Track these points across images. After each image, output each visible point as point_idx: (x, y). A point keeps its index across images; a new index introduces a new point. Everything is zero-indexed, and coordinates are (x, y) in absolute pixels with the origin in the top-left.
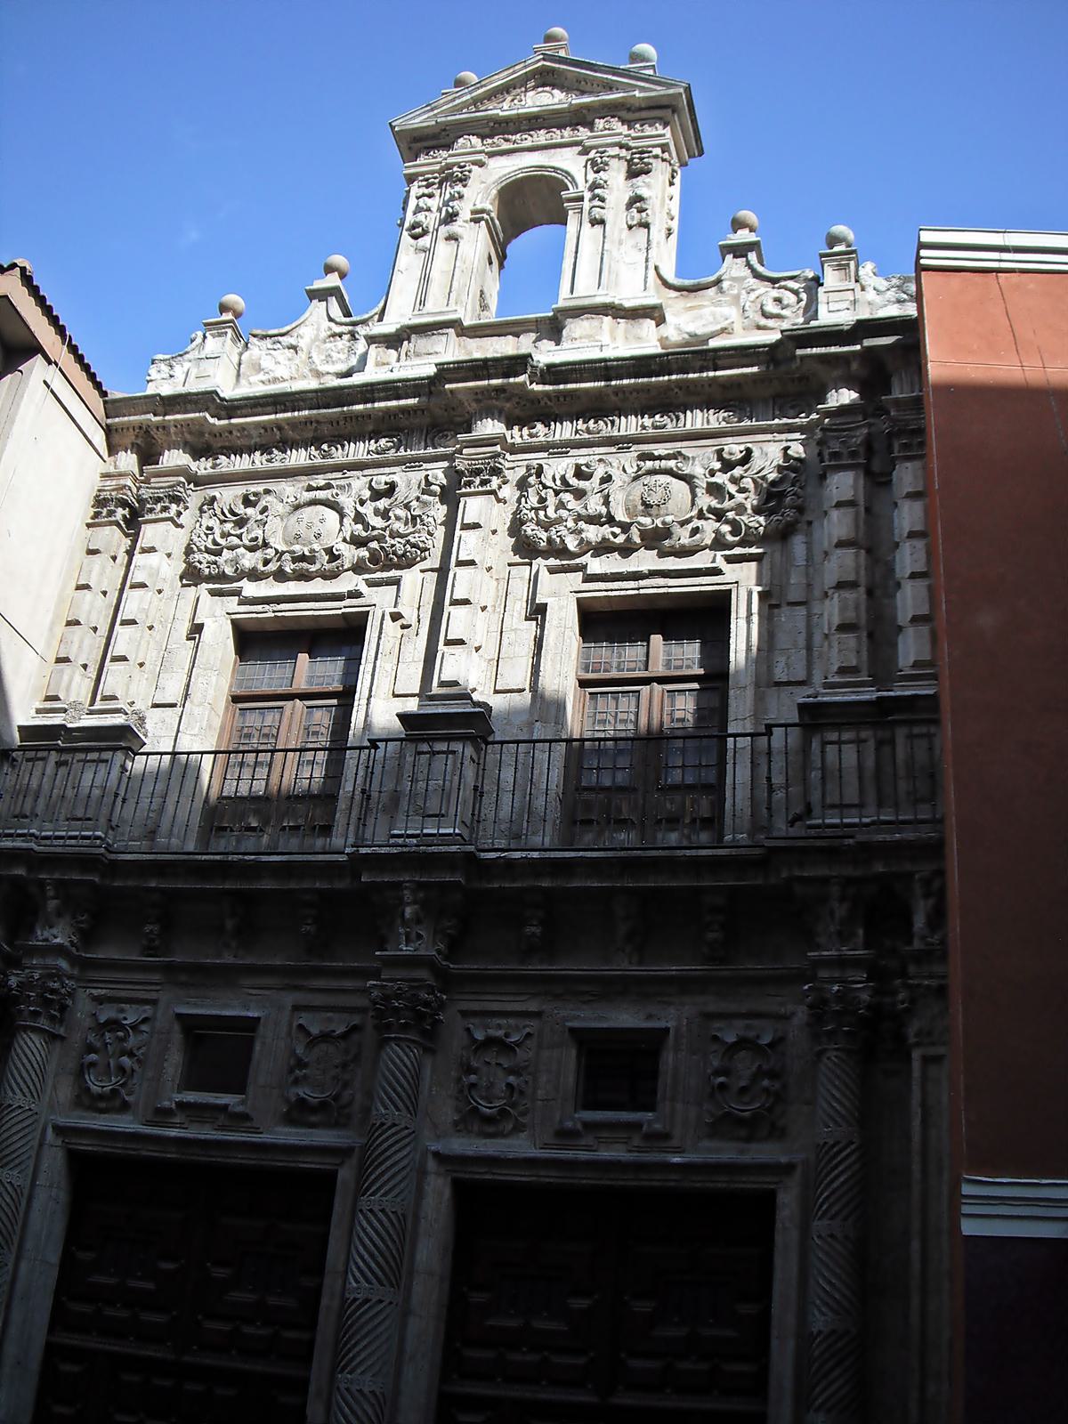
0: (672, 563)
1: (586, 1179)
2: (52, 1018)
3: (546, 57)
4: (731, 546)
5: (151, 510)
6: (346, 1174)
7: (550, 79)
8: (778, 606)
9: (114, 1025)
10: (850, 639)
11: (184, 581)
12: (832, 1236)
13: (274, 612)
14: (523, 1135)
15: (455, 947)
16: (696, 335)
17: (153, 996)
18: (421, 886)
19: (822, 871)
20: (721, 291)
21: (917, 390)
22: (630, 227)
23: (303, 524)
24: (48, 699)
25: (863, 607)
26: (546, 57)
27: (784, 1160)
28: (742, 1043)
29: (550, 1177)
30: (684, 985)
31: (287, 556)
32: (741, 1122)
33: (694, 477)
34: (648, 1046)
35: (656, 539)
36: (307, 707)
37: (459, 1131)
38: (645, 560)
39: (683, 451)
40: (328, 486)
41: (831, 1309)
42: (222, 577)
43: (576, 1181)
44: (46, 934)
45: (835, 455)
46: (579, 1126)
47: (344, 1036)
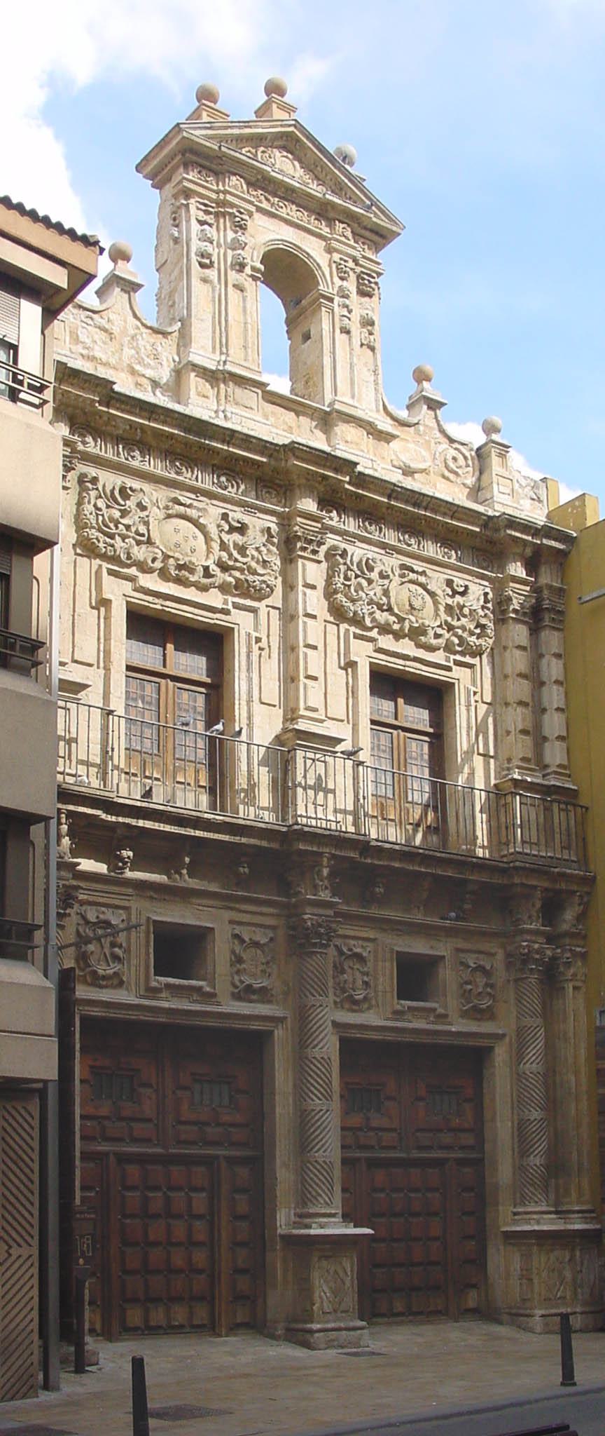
0: (421, 654)
1: (408, 1038)
3: (297, 125)
4: (455, 653)
7: (291, 146)
11: (79, 551)
13: (162, 606)
14: (371, 1011)
16: (409, 467)
17: (126, 904)
18: (333, 856)
20: (418, 433)
22: (362, 345)
26: (297, 125)
27: (500, 1032)
29: (390, 1037)
30: (451, 932)
31: (171, 561)
33: (437, 595)
34: (433, 962)
35: (416, 634)
36: (178, 688)
37: (337, 1008)
38: (406, 647)
39: (427, 571)
42: (114, 559)
43: (348, 1035)
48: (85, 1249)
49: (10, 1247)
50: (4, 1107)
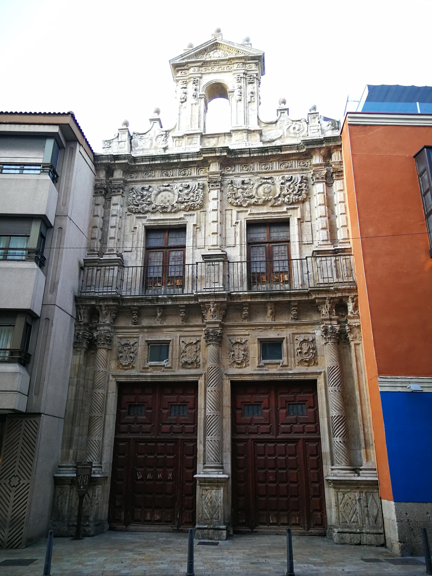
2: (108, 344)
5: (114, 192)
6: (201, 382)
8: (303, 222)
9: (127, 345)
10: (325, 232)
12: (335, 391)
15: (224, 318)
17: (138, 336)
18: (215, 302)
19: (324, 296)
21: (340, 159)
23: (163, 197)
24: (91, 250)
25: (328, 222)
27: (318, 371)
28: (305, 341)
29: (256, 378)
30: (287, 325)
32: (306, 361)
40: (168, 186)
41: (337, 410)
44: (104, 320)
45: (317, 178)
46: (263, 364)
47: (195, 344)
48: (85, 481)
49: (20, 480)
50: (26, 421)
